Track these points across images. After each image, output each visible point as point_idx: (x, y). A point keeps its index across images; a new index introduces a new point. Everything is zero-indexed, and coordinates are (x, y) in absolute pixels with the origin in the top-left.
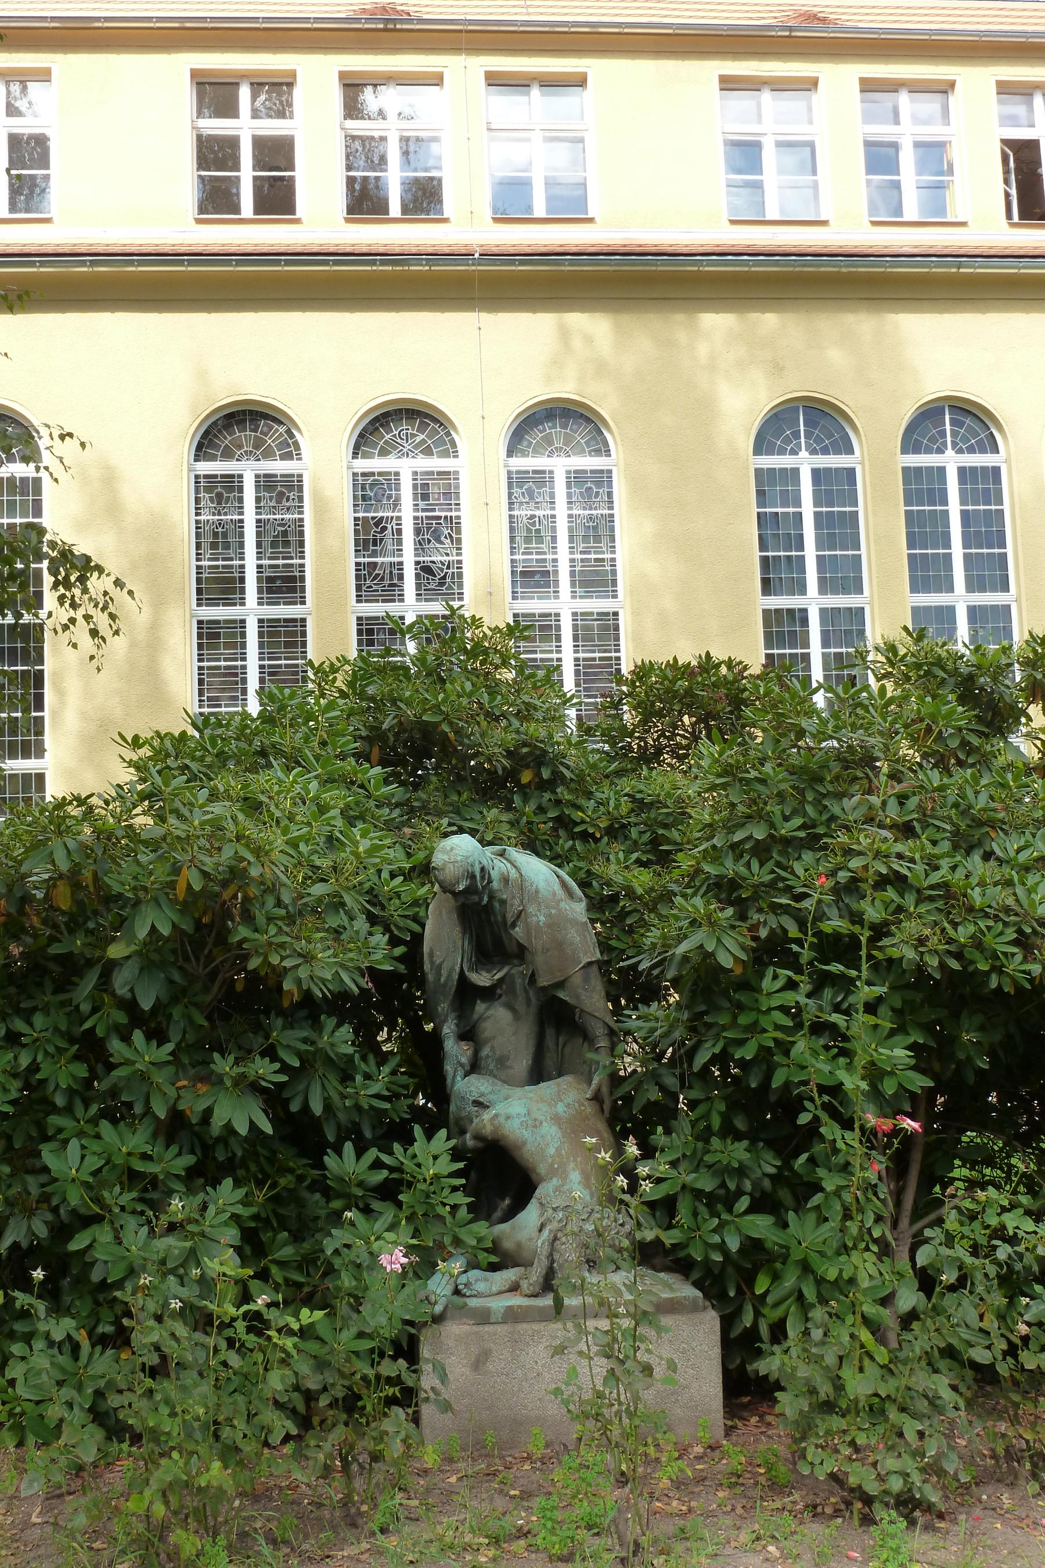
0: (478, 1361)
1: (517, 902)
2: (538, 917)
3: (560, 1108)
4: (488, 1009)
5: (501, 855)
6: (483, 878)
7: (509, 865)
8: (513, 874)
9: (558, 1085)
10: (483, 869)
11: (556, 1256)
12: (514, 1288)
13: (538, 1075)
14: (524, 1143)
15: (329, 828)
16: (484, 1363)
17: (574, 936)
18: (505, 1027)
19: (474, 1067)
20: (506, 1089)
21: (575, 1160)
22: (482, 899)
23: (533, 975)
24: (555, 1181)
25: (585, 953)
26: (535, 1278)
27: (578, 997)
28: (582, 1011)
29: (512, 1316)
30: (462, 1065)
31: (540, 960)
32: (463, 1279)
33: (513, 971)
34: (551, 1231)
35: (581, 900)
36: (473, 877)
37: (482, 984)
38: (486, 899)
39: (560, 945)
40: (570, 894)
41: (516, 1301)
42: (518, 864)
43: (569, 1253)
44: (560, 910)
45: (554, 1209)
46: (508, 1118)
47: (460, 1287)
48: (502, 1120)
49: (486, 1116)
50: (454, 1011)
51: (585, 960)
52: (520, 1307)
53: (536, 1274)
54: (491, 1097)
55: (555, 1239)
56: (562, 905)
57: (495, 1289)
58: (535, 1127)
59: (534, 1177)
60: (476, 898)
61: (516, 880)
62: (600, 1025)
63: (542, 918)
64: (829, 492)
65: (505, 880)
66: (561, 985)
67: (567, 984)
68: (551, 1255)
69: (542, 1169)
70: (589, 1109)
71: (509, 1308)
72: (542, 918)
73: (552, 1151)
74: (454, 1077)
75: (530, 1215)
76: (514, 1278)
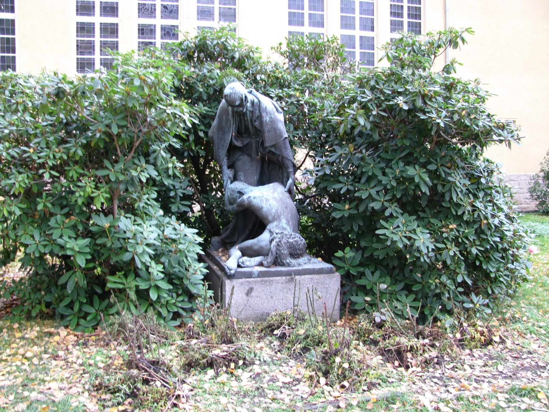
0: (248, 291)
1: (257, 112)
3: (276, 195)
4: (240, 156)
14: (262, 208)
15: (459, 90)
16: (251, 292)
19: (235, 179)
20: (251, 188)
28: (283, 157)
29: (261, 275)
30: (230, 178)
32: (241, 260)
36: (242, 100)
40: (277, 110)
46: (254, 198)
48: (252, 199)
53: (270, 259)
54: (245, 190)
59: (266, 222)
63: (268, 119)
64: (416, 27)
69: (270, 218)
71: (261, 272)
75: (265, 237)
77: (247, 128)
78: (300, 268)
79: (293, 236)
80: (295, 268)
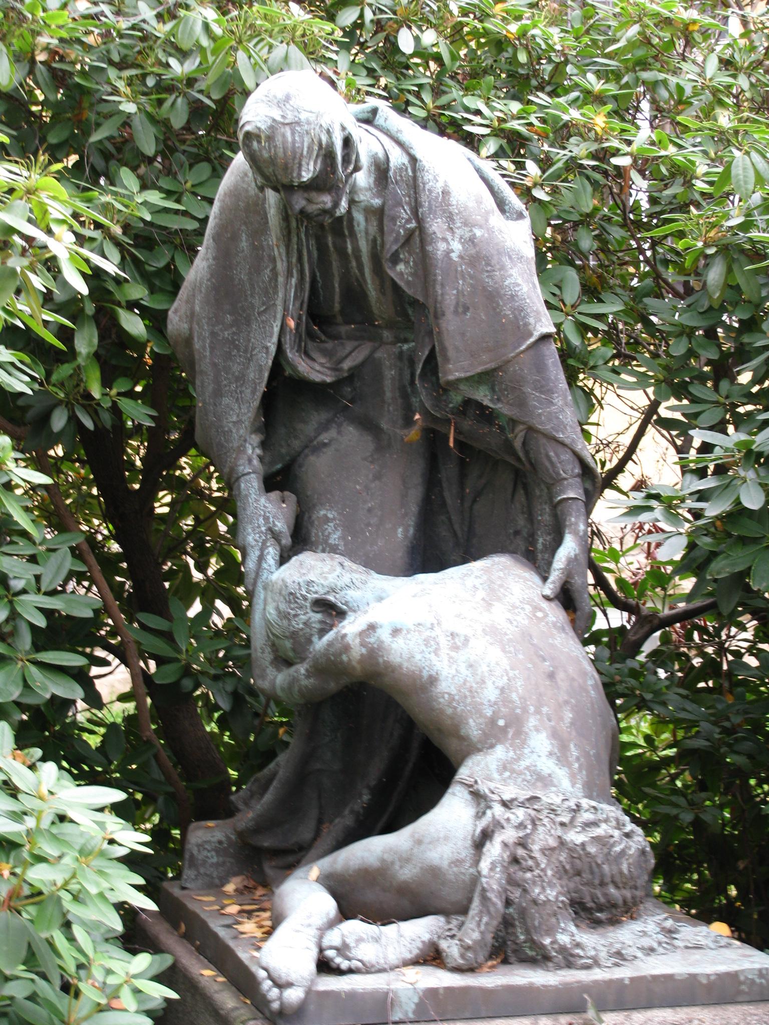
1: (404, 213)
4: (324, 427)
6: (346, 160)
9: (487, 571)
12: (432, 956)
14: (433, 680)
22: (336, 204)
23: (432, 358)
24: (500, 752)
26: (476, 935)
28: (531, 429)
30: (276, 536)
32: (333, 938)
33: (378, 355)
35: (520, 216)
37: (317, 377)
38: (344, 204)
40: (501, 204)
46: (396, 632)
47: (330, 953)
48: (384, 634)
49: (350, 627)
50: (256, 431)
52: (448, 990)
54: (352, 595)
57: (393, 957)
61: (401, 169)
62: (567, 456)
63: (456, 246)
69: (473, 729)
72: (456, 246)
74: (261, 558)
75: (449, 820)
76: (426, 937)
79: (587, 816)
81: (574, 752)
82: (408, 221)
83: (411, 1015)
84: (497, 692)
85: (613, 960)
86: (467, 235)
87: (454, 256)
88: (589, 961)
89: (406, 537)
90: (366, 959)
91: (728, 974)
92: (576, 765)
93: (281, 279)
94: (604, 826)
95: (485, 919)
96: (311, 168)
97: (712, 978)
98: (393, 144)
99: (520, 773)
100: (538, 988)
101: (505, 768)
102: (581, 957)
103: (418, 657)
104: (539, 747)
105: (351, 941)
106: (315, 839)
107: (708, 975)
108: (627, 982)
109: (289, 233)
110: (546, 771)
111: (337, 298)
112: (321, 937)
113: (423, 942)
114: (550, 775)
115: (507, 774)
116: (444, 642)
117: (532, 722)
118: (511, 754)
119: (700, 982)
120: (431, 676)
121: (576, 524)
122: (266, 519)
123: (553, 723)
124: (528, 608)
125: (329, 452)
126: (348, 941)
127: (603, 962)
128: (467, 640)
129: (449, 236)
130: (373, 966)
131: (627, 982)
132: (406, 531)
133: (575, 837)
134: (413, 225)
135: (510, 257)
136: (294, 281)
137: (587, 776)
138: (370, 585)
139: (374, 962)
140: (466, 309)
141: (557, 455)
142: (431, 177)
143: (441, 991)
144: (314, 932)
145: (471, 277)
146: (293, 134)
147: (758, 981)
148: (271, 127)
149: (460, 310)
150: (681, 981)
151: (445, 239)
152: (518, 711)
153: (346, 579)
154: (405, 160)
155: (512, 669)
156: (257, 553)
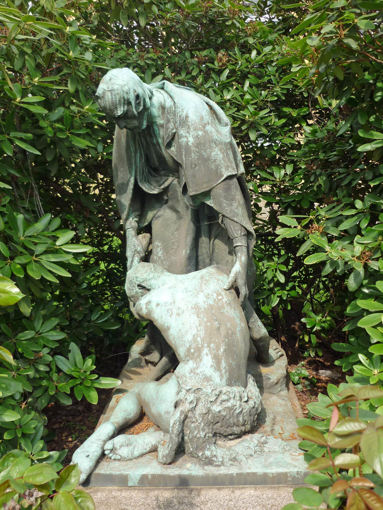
2: (188, 138)
5: (163, 88)
6: (138, 104)
7: (166, 95)
8: (169, 103)
10: (137, 97)
11: (187, 432)
13: (195, 263)
14: (168, 328)
17: (217, 154)
18: (173, 225)
21: (209, 346)
22: (141, 124)
24: (191, 364)
25: (227, 167)
27: (221, 205)
28: (223, 216)
31: (187, 174)
32: (109, 446)
34: (182, 412)
36: (129, 103)
39: (206, 160)
41: (153, 468)
42: (172, 94)
43: (198, 431)
44: (206, 132)
45: (188, 391)
46: (158, 305)
51: (226, 174)
54: (153, 282)
55: (186, 417)
56: (209, 128)
58: (178, 315)
60: (135, 123)
62: (238, 227)
63: (191, 140)
65: (163, 108)
66: (207, 194)
67: (212, 193)
68: (182, 431)
70: (227, 298)
73: (189, 337)
76: (154, 443)
77: (161, 158)
78: (234, 471)
79: (224, 397)
80: (223, 471)
81: (223, 364)
82: (172, 129)
83: (137, 484)
84: (192, 336)
85: (230, 462)
86: (196, 134)
87: (190, 144)
88: (220, 463)
89: (186, 254)
90: (122, 455)
91: (282, 473)
92: (224, 371)
93: (133, 154)
94: (232, 401)
95: (170, 446)
96: (122, 109)
97: (274, 475)
98: (169, 97)
99: (198, 374)
100: (194, 476)
101: (192, 372)
102: (216, 462)
103: (164, 317)
104: (207, 361)
105: (117, 446)
106: (159, 361)
107: (273, 474)
108: (235, 475)
109: (135, 136)
110: (208, 375)
111: (156, 161)
112: (104, 444)
113: (152, 445)
114: (210, 376)
115: (192, 374)
116: (175, 311)
117: (206, 351)
118: (195, 365)
119: (269, 477)
120: (168, 326)
121: (241, 257)
122: (134, 246)
123: (215, 352)
124: (215, 295)
125: (160, 219)
126: (116, 446)
127: (226, 464)
128: (183, 312)
129: (188, 135)
130: (125, 458)
131: (235, 475)
132: (186, 252)
133: (216, 408)
134: (174, 131)
135: (215, 143)
136: (138, 155)
137: (229, 375)
138: (161, 278)
139: (126, 456)
140: (196, 166)
141: (234, 228)
142: (180, 110)
143: (150, 477)
144: (101, 443)
145: (197, 152)
146: (111, 95)
147: (296, 476)
148: (103, 93)
149: (193, 166)
150: (260, 475)
151: (186, 137)
152: (200, 346)
153: (151, 276)
154: (172, 103)
155: (200, 326)
156: (131, 259)
